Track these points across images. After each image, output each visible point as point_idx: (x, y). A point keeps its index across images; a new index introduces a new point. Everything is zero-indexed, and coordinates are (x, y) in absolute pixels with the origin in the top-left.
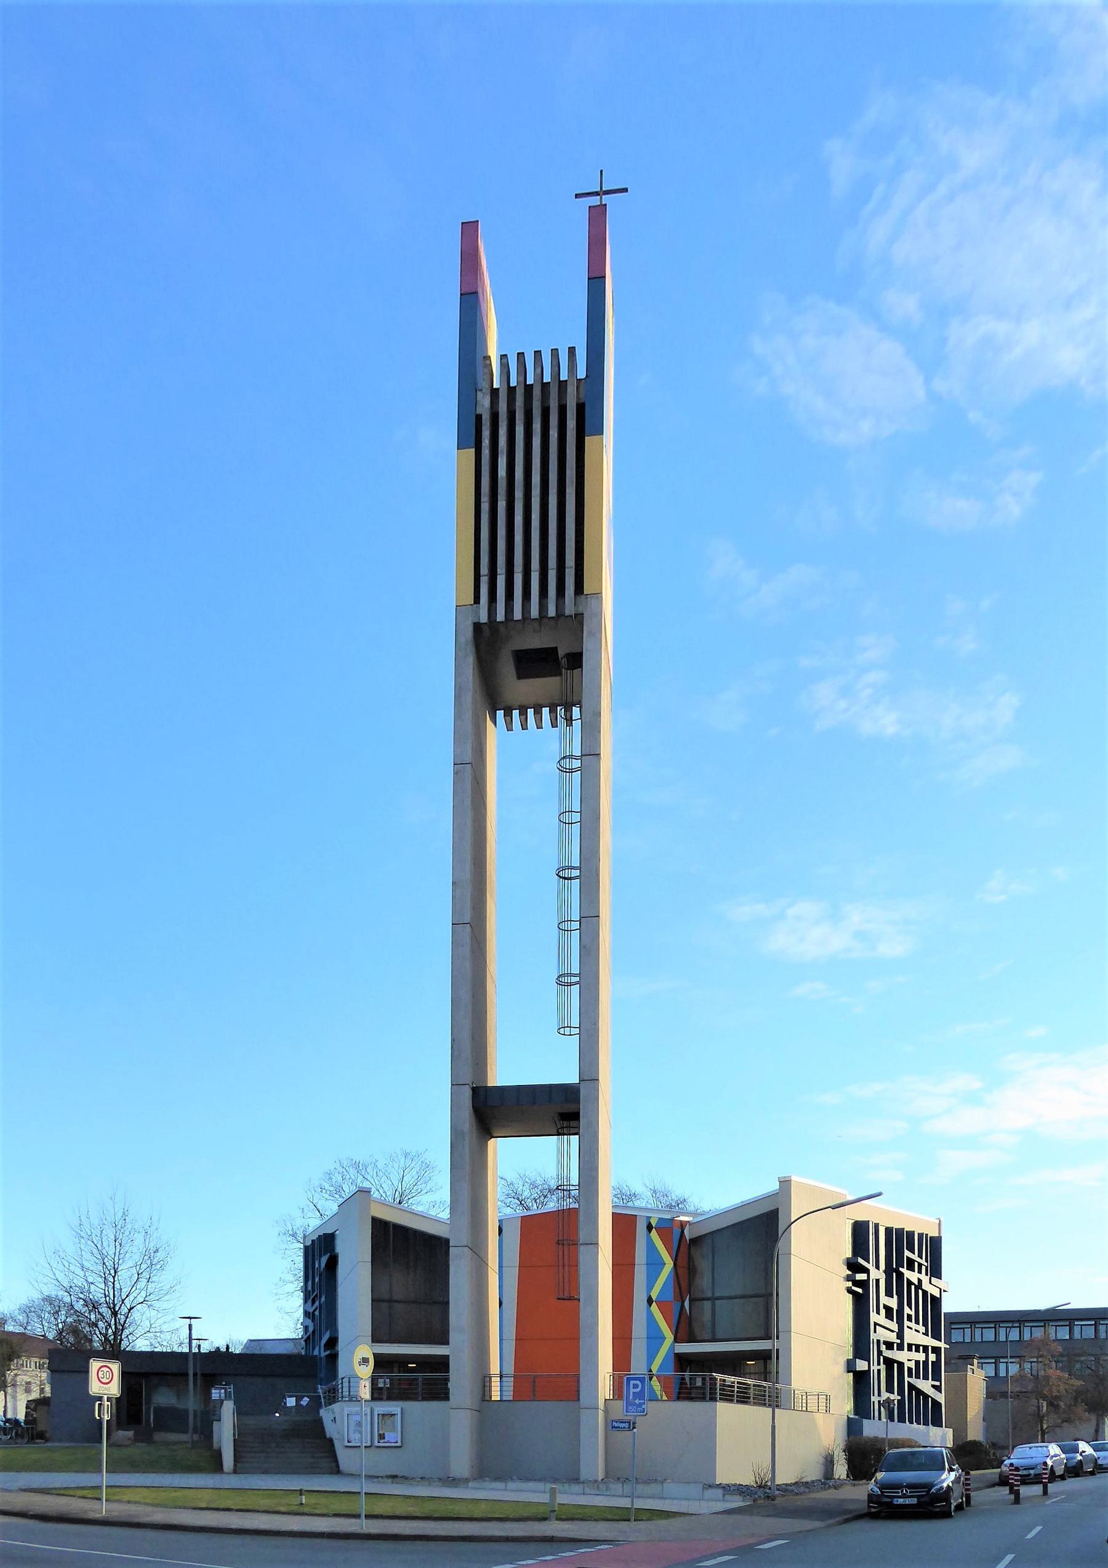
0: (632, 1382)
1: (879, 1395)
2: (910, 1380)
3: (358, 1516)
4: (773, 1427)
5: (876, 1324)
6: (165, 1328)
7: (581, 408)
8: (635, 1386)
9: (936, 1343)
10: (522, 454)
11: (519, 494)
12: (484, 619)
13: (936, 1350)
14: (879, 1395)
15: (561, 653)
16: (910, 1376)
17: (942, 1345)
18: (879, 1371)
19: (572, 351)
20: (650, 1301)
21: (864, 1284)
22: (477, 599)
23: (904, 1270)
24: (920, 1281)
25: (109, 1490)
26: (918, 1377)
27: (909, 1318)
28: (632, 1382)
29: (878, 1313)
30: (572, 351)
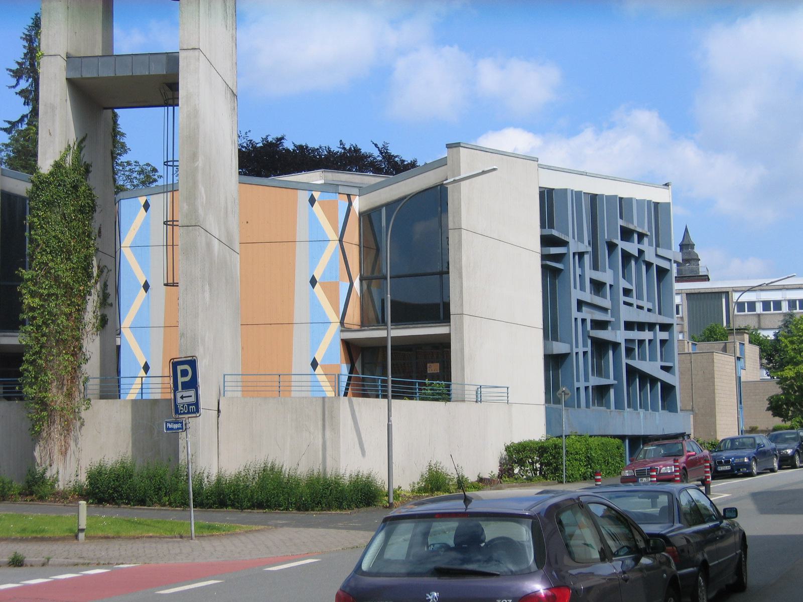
0: (180, 368)
1: (587, 379)
2: (631, 362)
8: (184, 373)
13: (665, 327)
14: (587, 379)
18: (585, 353)
20: (313, 282)
21: (558, 258)
24: (641, 252)
26: (642, 358)
27: (627, 292)
28: (180, 368)
29: (583, 288)
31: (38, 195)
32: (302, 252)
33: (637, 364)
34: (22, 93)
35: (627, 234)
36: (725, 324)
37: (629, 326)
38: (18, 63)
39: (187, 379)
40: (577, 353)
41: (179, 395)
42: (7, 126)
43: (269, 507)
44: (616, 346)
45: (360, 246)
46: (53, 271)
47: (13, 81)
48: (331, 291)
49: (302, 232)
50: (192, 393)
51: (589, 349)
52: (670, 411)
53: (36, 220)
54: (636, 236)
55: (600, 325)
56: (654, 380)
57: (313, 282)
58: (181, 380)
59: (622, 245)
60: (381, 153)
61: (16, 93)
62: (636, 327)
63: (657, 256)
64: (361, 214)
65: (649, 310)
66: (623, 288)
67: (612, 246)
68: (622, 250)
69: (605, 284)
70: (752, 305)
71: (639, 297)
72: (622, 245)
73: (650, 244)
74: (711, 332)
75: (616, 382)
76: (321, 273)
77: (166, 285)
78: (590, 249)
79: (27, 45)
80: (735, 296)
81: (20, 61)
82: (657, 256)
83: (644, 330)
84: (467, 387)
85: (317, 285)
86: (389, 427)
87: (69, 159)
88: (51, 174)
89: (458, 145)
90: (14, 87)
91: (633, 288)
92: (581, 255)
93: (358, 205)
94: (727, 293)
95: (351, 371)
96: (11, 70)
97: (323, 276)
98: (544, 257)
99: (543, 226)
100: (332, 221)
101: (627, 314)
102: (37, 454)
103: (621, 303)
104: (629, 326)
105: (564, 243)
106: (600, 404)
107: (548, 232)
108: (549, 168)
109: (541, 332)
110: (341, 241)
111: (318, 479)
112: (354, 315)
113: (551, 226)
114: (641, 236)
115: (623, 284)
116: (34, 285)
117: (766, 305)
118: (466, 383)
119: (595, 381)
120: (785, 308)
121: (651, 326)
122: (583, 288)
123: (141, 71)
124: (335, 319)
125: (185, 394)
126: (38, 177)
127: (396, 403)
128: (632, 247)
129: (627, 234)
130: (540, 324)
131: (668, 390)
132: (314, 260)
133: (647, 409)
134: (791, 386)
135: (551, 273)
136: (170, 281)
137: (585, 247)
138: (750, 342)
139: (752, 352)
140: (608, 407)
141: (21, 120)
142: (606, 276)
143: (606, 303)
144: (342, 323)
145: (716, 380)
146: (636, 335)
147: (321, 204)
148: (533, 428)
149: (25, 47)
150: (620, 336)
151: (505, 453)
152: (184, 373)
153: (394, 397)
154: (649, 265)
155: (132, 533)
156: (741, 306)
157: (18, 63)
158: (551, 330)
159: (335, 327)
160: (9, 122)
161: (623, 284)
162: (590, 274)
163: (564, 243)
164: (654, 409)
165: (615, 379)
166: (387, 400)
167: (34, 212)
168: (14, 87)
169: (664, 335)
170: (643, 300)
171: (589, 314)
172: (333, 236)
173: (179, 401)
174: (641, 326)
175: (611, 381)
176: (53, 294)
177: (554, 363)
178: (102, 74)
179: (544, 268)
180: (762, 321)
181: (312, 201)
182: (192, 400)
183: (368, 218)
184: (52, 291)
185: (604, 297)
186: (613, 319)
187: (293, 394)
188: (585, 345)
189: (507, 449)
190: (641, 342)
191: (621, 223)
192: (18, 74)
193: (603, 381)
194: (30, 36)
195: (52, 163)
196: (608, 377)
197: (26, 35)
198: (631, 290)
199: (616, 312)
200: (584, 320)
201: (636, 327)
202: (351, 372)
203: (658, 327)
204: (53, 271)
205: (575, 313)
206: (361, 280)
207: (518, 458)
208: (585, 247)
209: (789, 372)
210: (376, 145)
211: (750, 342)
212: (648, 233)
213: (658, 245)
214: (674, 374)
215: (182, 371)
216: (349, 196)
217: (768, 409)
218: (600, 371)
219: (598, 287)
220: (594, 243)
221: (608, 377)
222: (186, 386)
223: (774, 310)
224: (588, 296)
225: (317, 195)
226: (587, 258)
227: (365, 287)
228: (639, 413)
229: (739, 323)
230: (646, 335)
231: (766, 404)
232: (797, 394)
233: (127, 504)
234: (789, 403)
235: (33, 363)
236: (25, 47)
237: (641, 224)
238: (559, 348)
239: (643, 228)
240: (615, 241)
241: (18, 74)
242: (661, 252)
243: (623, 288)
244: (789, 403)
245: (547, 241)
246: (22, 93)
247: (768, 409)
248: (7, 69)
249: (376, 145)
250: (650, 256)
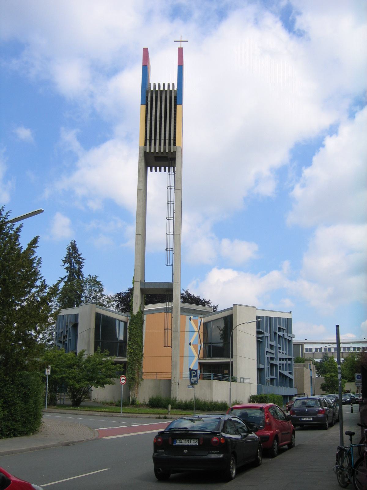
0: (192, 372)
1: (268, 377)
2: (280, 371)
3: (120, 412)
4: (230, 389)
5: (267, 352)
6: (348, 372)
7: (175, 97)
8: (194, 373)
9: (290, 357)
10: (159, 106)
11: (158, 119)
12: (148, 151)
13: (290, 359)
14: (268, 377)
15: (168, 158)
16: (280, 369)
17: (293, 358)
18: (268, 368)
19: (173, 84)
20: (190, 344)
21: (261, 338)
22: (146, 145)
23: (277, 332)
24: (283, 335)
25: (294, 345)
26: (283, 370)
27: (279, 348)
28: (192, 372)
29: (268, 348)
30: (173, 84)
31: (133, 321)
32: (187, 335)
33: (282, 371)
34: (67, 268)
35: (280, 329)
36: (301, 357)
37: (280, 359)
38: (65, 258)
39: (194, 375)
40: (266, 368)
41: (192, 379)
42: (60, 279)
43: (200, 410)
44: (276, 365)
45: (203, 333)
46: (137, 342)
47: (63, 264)
48: (195, 347)
49: (187, 329)
50: (196, 378)
51: (269, 367)
52: (291, 388)
53: (132, 328)
54: (282, 330)
55: (272, 359)
56: (286, 377)
57: (190, 344)
58: (192, 375)
59: (279, 333)
60: (186, 293)
61: (64, 268)
62: (285, 360)
63: (288, 336)
64: (204, 323)
65: (285, 354)
66: (270, 344)
67: (275, 333)
68: (278, 335)
69: (273, 345)
70: (311, 349)
71: (283, 350)
72: (279, 333)
73: (286, 332)
74: (297, 359)
75: (276, 377)
76: (192, 342)
77: (164, 347)
78: (270, 335)
79: (68, 251)
80: (306, 346)
81: (66, 257)
82: (288, 336)
83: (284, 361)
84: (238, 378)
85: (191, 345)
86: (230, 389)
87: (62, 285)
88: (137, 315)
89: (237, 305)
90: (63, 266)
91: (281, 347)
92: (267, 337)
93: (203, 320)
94: (302, 344)
95: (201, 371)
96: (63, 260)
97: (193, 342)
98: (258, 338)
99: (257, 328)
100: (196, 325)
101: (280, 355)
102: (131, 394)
103: (278, 352)
104: (280, 359)
105: (263, 333)
106: (271, 384)
107: (259, 330)
108: (259, 309)
109: (256, 361)
110: (199, 332)
111: (216, 403)
112: (201, 355)
113: (259, 328)
114: (284, 330)
115: (279, 346)
116: (132, 346)
117: (316, 349)
118: (184, 372)
119: (271, 377)
120: (323, 351)
121: (286, 359)
122: (268, 348)
123: (161, 287)
124: (196, 355)
125: (194, 378)
126: (133, 316)
127: (232, 383)
128: (281, 334)
129: (280, 329)
130: (256, 358)
131: (291, 380)
132: (191, 337)
133: (284, 387)
134: (328, 380)
135: (259, 343)
136: (165, 346)
137: (268, 334)
138: (313, 364)
139: (313, 367)
140: (274, 385)
141: (65, 277)
142: (273, 343)
143: (274, 352)
144: (199, 357)
145: (304, 377)
146: (282, 362)
147: (194, 321)
148: (254, 393)
149: (67, 252)
150: (277, 362)
151: (250, 398)
152: (194, 373)
153: (232, 381)
154: (285, 339)
155: (180, 413)
156: (307, 349)
157: (65, 258)
158: (259, 361)
159: (197, 358)
160: (61, 278)
161: (279, 346)
162: (270, 343)
163: (263, 333)
164: (287, 387)
165: (276, 376)
166: (229, 382)
167: (132, 325)
168: (63, 266)
169: (289, 362)
170: (280, 350)
171: (269, 356)
172: (196, 330)
173: (192, 380)
174: (283, 359)
175: (275, 377)
176: (137, 349)
177: (260, 370)
178: (146, 287)
179: (257, 341)
180: (315, 355)
181: (190, 319)
182: (196, 380)
183: (206, 325)
184: (137, 348)
185: (273, 350)
186: (275, 357)
187: (183, 378)
188: (268, 366)
189: (250, 397)
190: (283, 364)
191: (278, 326)
192: (65, 262)
193: (273, 377)
194: (69, 248)
195: (137, 312)
196: (274, 376)
197: (68, 248)
198: (280, 347)
199: (276, 355)
200: (268, 357)
201: (285, 360)
202: (200, 372)
203: (288, 359)
204: (137, 342)
205: (266, 356)
206: (203, 343)
207: (253, 399)
208: (268, 334)
209: (328, 375)
210: (184, 290)
211: (313, 364)
212: (286, 329)
213: (288, 333)
214: (292, 375)
215: (194, 373)
216: (201, 318)
217: (321, 388)
218: (272, 374)
219: (271, 346)
220: (270, 333)
221: (274, 376)
222: (194, 377)
223: (319, 351)
224: (269, 350)
225: (192, 317)
226: (269, 338)
227: (204, 346)
228: (282, 388)
229: (306, 357)
230: (284, 362)
231: (320, 386)
232: (330, 383)
233: (161, 408)
234: (328, 386)
235: (131, 368)
236: (67, 252)
237: (283, 326)
238: (262, 366)
239: (284, 327)
240: (277, 332)
241: (65, 262)
242: (289, 335)
243: (270, 344)
244: (328, 386)
245: (258, 333)
246: (67, 268)
247: (321, 388)
248: (62, 260)
249: (184, 290)
250: (286, 337)
